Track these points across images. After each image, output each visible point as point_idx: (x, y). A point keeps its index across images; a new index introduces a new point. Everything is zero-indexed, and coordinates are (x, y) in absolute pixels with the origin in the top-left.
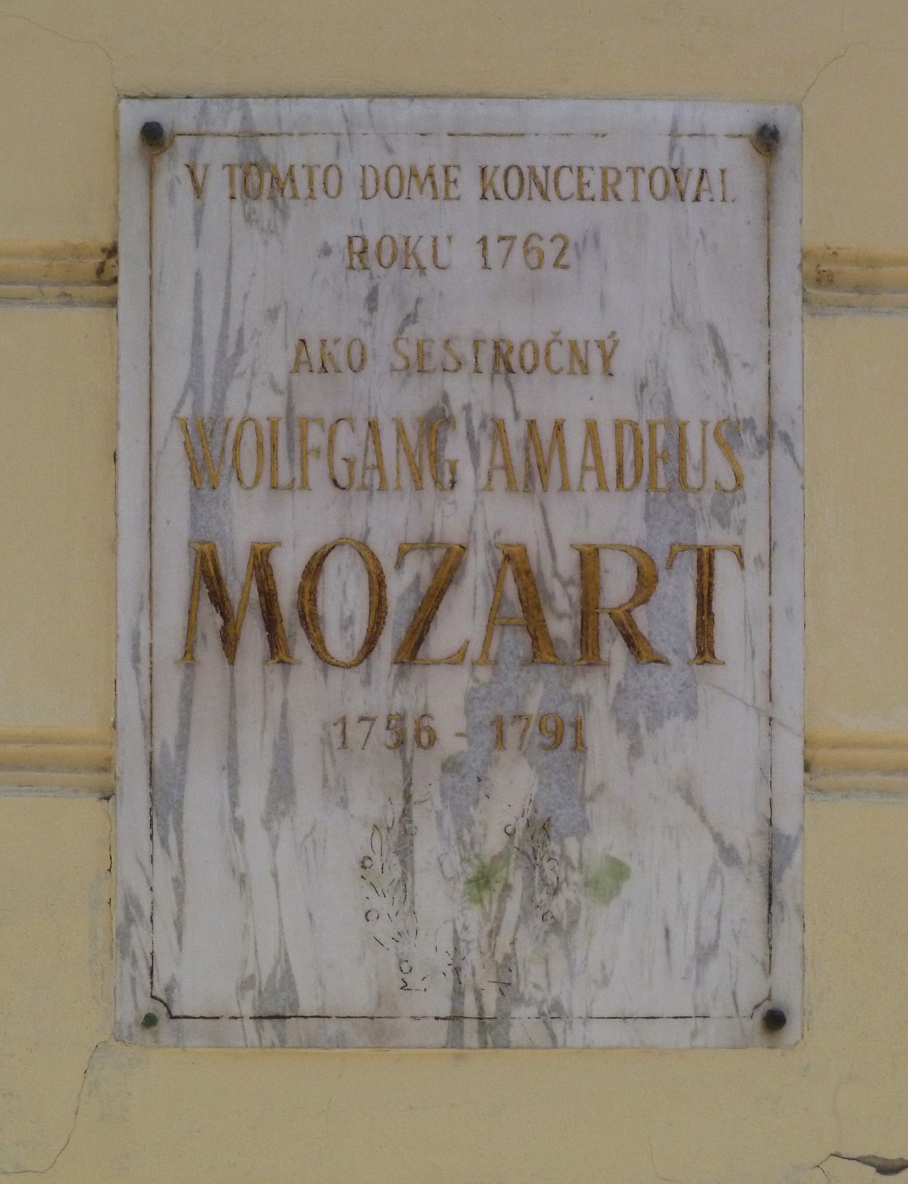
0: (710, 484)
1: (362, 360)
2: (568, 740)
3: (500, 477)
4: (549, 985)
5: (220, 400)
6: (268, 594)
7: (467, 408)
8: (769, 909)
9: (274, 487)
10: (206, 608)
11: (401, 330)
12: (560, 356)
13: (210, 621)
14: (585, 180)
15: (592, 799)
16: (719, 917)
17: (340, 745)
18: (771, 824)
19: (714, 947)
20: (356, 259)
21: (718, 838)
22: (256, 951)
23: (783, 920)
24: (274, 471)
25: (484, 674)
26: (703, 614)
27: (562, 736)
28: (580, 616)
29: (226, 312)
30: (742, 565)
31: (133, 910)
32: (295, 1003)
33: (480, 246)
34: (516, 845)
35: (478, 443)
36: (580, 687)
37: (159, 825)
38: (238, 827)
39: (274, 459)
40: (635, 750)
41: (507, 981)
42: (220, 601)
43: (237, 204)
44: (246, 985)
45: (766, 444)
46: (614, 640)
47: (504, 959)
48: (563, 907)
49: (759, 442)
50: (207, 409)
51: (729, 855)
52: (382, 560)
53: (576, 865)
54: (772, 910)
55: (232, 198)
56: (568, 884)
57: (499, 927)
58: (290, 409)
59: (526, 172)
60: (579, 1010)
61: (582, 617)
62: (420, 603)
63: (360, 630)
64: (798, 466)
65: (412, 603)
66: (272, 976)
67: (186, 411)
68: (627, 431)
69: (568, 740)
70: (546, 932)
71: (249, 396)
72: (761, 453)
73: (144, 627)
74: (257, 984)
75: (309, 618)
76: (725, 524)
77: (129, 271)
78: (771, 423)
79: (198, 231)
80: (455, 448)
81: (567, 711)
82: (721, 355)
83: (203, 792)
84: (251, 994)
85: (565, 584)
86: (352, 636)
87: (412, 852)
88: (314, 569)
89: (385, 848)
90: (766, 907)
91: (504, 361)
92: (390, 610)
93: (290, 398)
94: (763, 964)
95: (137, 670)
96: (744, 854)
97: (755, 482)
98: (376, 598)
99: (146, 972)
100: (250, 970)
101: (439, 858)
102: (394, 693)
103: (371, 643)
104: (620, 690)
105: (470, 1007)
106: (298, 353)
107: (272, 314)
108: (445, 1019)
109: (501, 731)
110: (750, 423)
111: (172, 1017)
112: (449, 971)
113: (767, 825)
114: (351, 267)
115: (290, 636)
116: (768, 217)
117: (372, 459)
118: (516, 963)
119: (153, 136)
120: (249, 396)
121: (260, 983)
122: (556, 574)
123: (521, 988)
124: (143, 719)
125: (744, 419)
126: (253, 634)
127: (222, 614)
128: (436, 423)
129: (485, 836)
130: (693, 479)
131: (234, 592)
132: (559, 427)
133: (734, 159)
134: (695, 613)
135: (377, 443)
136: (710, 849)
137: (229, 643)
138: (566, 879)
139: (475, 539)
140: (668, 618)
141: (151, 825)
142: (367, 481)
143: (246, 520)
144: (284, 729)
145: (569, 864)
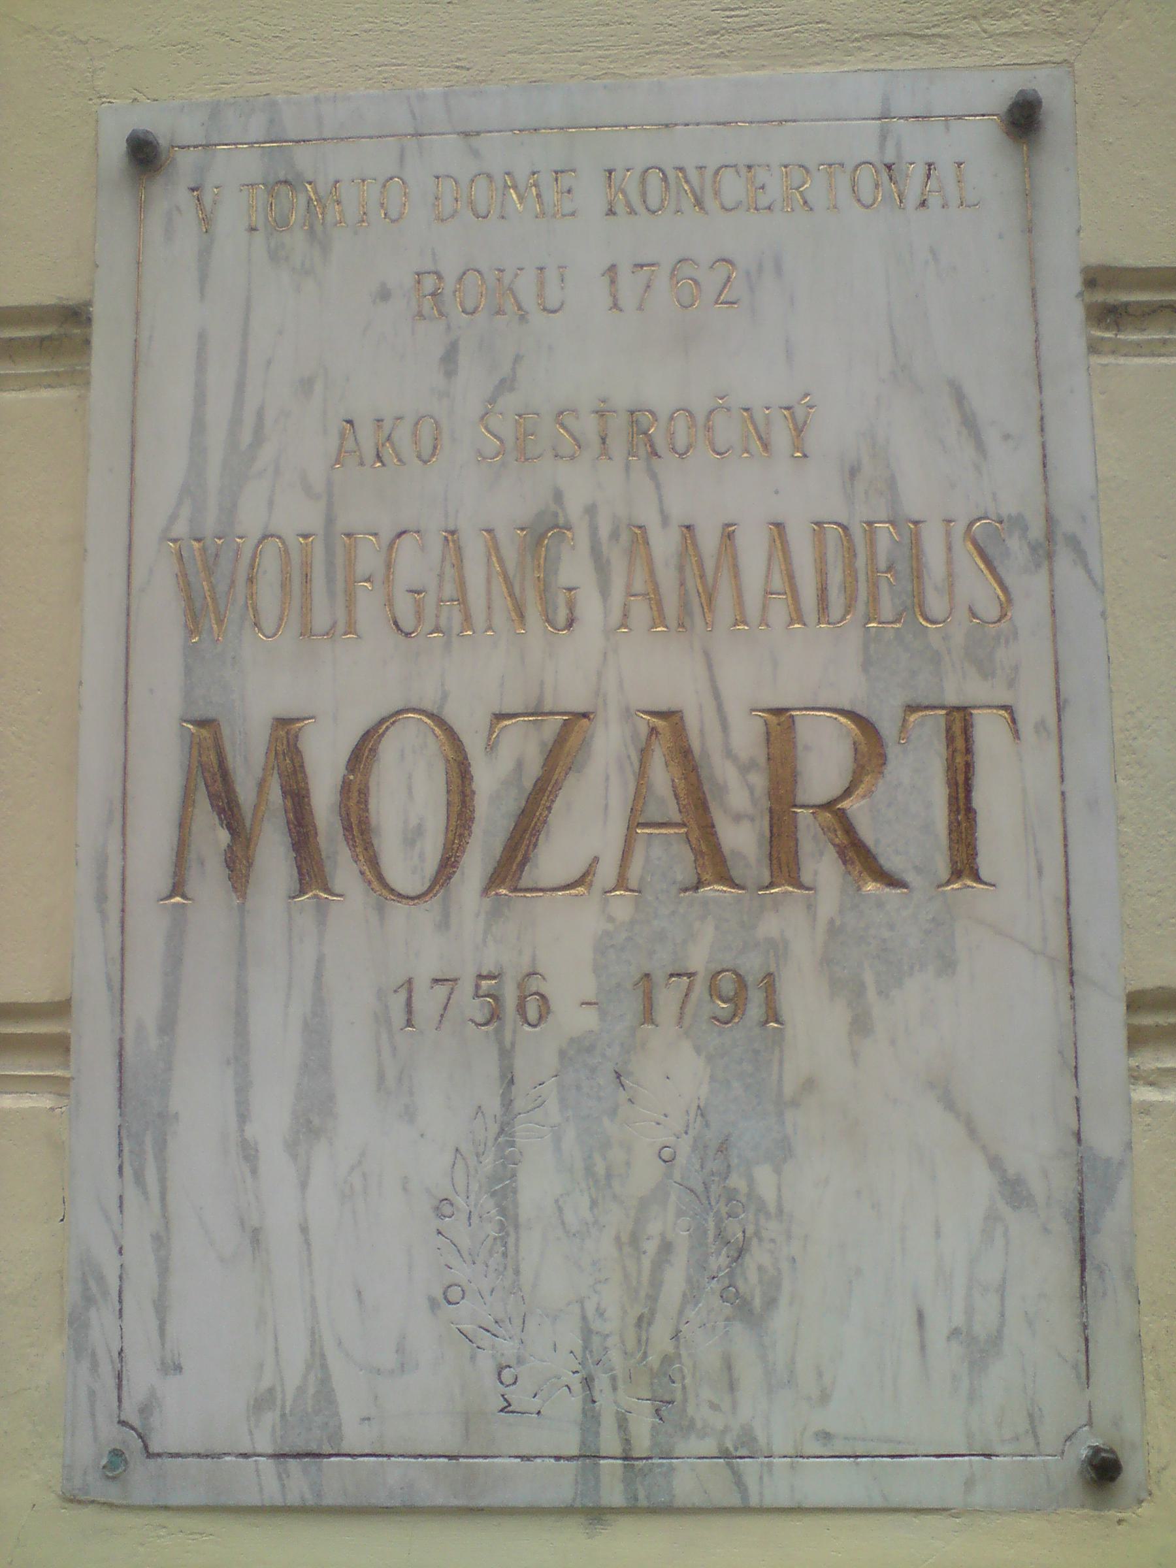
0: (962, 613)
1: (435, 448)
2: (755, 1010)
3: (641, 611)
4: (734, 1406)
5: (230, 511)
6: (298, 795)
7: (591, 511)
8: (1082, 1277)
9: (306, 632)
10: (205, 816)
11: (492, 401)
12: (727, 431)
13: (212, 837)
14: (758, 183)
15: (795, 1103)
16: (1001, 1290)
17: (403, 1022)
18: (1079, 1141)
19: (997, 1339)
20: (428, 302)
21: (995, 1163)
22: (277, 1350)
23: (1105, 1294)
24: (306, 609)
25: (622, 905)
26: (958, 811)
27: (744, 999)
28: (767, 818)
29: (240, 387)
30: (1016, 734)
31: (92, 1284)
32: (336, 1435)
33: (606, 279)
34: (677, 1176)
35: (608, 561)
36: (769, 926)
37: (131, 1152)
38: (249, 1153)
39: (307, 595)
40: (861, 1025)
41: (667, 1398)
42: (228, 810)
43: (259, 237)
44: (261, 1403)
45: (1045, 552)
46: (821, 854)
47: (662, 1362)
48: (753, 1276)
49: (1034, 549)
50: (210, 523)
51: (1014, 1190)
52: (466, 739)
53: (772, 1207)
54: (1087, 1279)
55: (253, 229)
56: (760, 1240)
57: (653, 1312)
58: (330, 521)
59: (671, 174)
60: (781, 1443)
61: (771, 818)
62: (524, 803)
63: (432, 848)
64: (1095, 584)
65: (512, 804)
66: (301, 1390)
67: (181, 529)
68: (832, 531)
69: (755, 1010)
70: (727, 1319)
71: (271, 503)
72: (1038, 566)
73: (114, 847)
74: (279, 1402)
75: (358, 827)
76: (986, 670)
77: (107, 338)
78: (1050, 520)
79: (203, 278)
80: (574, 569)
81: (752, 965)
82: (970, 424)
83: (198, 1096)
84: (270, 1418)
85: (745, 769)
86: (422, 856)
87: (515, 1191)
88: (362, 755)
89: (475, 1187)
90: (1077, 1273)
91: (641, 437)
92: (477, 815)
93: (330, 505)
94: (1075, 1367)
95: (103, 913)
96: (1037, 1186)
97: (1030, 610)
98: (456, 799)
99: (111, 1382)
100: (267, 1381)
101: (557, 1201)
102: (484, 941)
103: (448, 864)
104: (834, 930)
105: (610, 1442)
106: (342, 436)
107: (306, 385)
108: (569, 1458)
109: (650, 999)
110: (1018, 523)
111: (150, 1456)
112: (575, 1381)
113: (1074, 1141)
114: (420, 315)
115: (329, 857)
116: (1029, 228)
117: (449, 590)
118: (681, 1370)
119: (144, 154)
120: (271, 503)
121: (284, 1400)
122: (729, 754)
123: (691, 1410)
124: (110, 988)
125: (1010, 516)
126: (273, 854)
127: (229, 827)
128: (544, 533)
129: (628, 1164)
130: (936, 604)
131: (246, 793)
132: (728, 535)
133: (979, 143)
134: (945, 811)
135: (459, 565)
136: (984, 1180)
137: (238, 866)
138: (757, 1234)
139: (605, 704)
140: (905, 810)
141: (121, 1151)
142: (443, 622)
143: (264, 685)
144: (319, 1000)
145: (762, 1208)
